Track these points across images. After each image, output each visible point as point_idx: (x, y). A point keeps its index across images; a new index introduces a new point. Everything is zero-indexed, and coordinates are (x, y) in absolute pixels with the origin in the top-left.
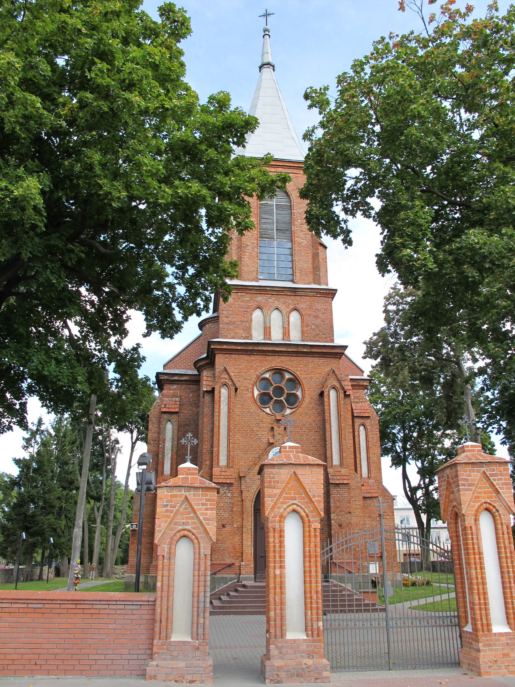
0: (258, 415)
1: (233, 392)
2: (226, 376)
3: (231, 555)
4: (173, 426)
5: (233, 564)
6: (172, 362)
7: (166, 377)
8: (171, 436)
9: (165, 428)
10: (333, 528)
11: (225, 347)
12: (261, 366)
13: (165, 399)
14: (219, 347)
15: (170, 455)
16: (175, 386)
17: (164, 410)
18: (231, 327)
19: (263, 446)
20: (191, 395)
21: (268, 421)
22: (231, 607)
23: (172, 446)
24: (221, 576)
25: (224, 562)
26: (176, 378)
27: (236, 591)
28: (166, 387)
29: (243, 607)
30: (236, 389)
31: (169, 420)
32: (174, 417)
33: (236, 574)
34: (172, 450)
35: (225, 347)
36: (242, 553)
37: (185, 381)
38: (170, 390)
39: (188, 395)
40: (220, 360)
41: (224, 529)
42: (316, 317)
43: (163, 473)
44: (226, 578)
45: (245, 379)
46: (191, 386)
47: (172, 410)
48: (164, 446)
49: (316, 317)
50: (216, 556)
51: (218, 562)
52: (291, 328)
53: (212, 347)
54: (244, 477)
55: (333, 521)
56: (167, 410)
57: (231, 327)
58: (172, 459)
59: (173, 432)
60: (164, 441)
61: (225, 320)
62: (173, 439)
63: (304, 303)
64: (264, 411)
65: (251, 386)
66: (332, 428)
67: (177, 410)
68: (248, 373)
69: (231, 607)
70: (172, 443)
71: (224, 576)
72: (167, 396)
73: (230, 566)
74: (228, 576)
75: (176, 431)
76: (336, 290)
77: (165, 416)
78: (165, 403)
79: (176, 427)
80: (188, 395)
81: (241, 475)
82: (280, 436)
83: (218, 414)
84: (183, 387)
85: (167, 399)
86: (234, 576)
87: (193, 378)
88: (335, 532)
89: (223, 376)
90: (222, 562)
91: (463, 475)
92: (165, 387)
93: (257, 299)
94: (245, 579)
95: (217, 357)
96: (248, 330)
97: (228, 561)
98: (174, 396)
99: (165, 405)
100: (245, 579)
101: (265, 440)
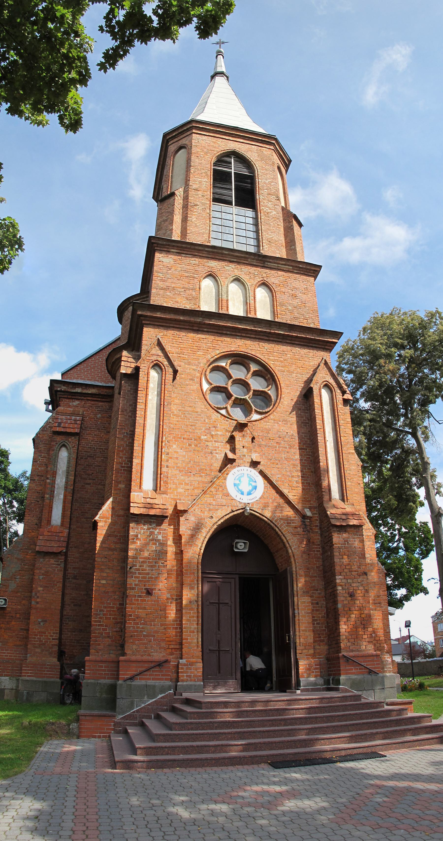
0: (209, 417)
1: (170, 376)
2: (160, 353)
3: (163, 644)
4: (69, 454)
5: (166, 661)
6: (75, 370)
7: (64, 388)
8: (65, 468)
9: (57, 456)
10: (340, 598)
11: (158, 315)
12: (214, 348)
13: (60, 417)
14: (149, 314)
15: (62, 497)
16: (76, 403)
17: (58, 429)
18: (168, 294)
19: (218, 465)
20: (99, 416)
21: (224, 428)
22: (173, 750)
23: (67, 482)
24: (143, 682)
25: (149, 658)
26: (79, 390)
27: (174, 710)
28: (63, 402)
29: (200, 749)
30: (175, 372)
31: (64, 446)
32: (73, 441)
33: (171, 680)
34: (66, 488)
35: (158, 315)
36: (181, 644)
37: (92, 395)
38: (69, 406)
39: (95, 415)
40: (150, 335)
41: (150, 598)
42: (294, 296)
43: (49, 521)
44: (154, 686)
45: (189, 364)
46: (100, 404)
47: (68, 430)
48: (54, 482)
49: (294, 296)
50: (134, 647)
51: (139, 657)
52: (257, 305)
53: (139, 313)
54: (185, 511)
55: (340, 588)
56: (62, 430)
57: (168, 294)
58: (64, 502)
59: (69, 462)
60: (54, 474)
61: (161, 284)
62: (68, 472)
63: (275, 277)
64: (218, 412)
65: (198, 375)
66: (328, 444)
67: (77, 431)
68: (195, 352)
69: (173, 750)
70: (67, 478)
71: (150, 682)
72: (63, 414)
73: (160, 664)
74: (157, 683)
75: (73, 462)
76: (320, 267)
77: (59, 439)
78: (59, 421)
79: (74, 456)
80: (95, 415)
81: (180, 508)
82: (245, 450)
83: (143, 407)
84: (89, 404)
85: (64, 417)
86: (168, 683)
87: (104, 392)
88: (344, 606)
89: (153, 352)
90: (145, 658)
91: (183, 676)
92: (61, 403)
93: (208, 265)
94: (188, 689)
95: (145, 329)
96: (197, 299)
97: (158, 656)
98: (73, 414)
99: (60, 424)
100: (188, 689)
101: (221, 457)
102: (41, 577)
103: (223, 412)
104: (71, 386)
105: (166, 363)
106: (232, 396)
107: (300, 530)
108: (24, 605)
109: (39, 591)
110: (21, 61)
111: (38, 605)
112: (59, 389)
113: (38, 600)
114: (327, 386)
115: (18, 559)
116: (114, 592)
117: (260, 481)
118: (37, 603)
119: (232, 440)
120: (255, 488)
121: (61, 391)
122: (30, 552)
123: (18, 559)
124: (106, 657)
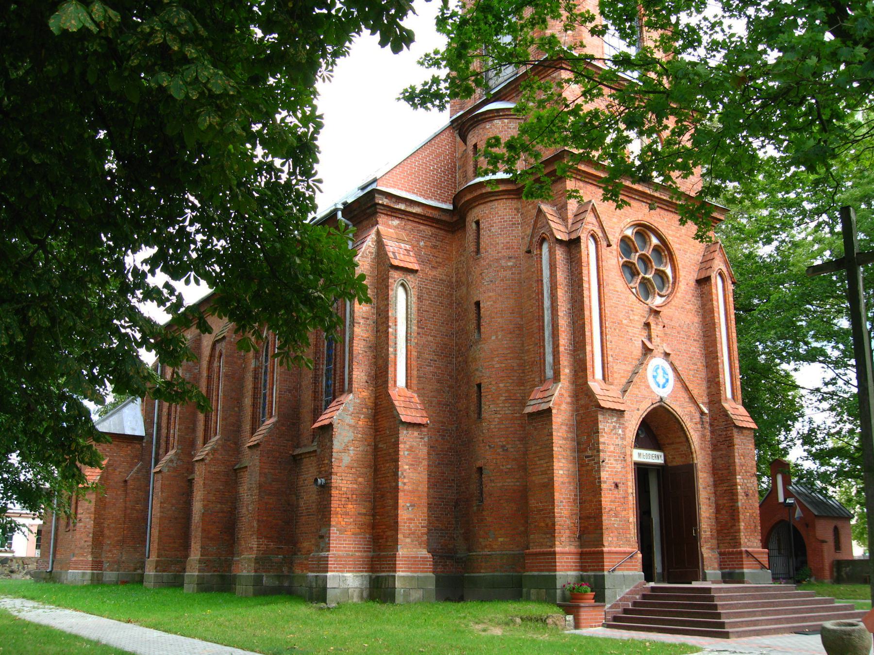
16: (396, 222)
26: (402, 206)
46: (422, 227)
80: (418, 241)
84: (410, 225)
88: (743, 504)
102: (406, 453)
103: (634, 290)
104: (394, 200)
105: (600, 235)
106: (639, 274)
107: (699, 426)
108: (360, 483)
109: (405, 470)
110: (748, 67)
111: (406, 487)
112: (380, 202)
113: (405, 480)
114: (721, 274)
115: (350, 426)
116: (570, 483)
117: (671, 375)
118: (405, 484)
119: (647, 325)
120: (667, 381)
121: (382, 205)
122: (362, 416)
123: (350, 426)
124: (567, 549)
